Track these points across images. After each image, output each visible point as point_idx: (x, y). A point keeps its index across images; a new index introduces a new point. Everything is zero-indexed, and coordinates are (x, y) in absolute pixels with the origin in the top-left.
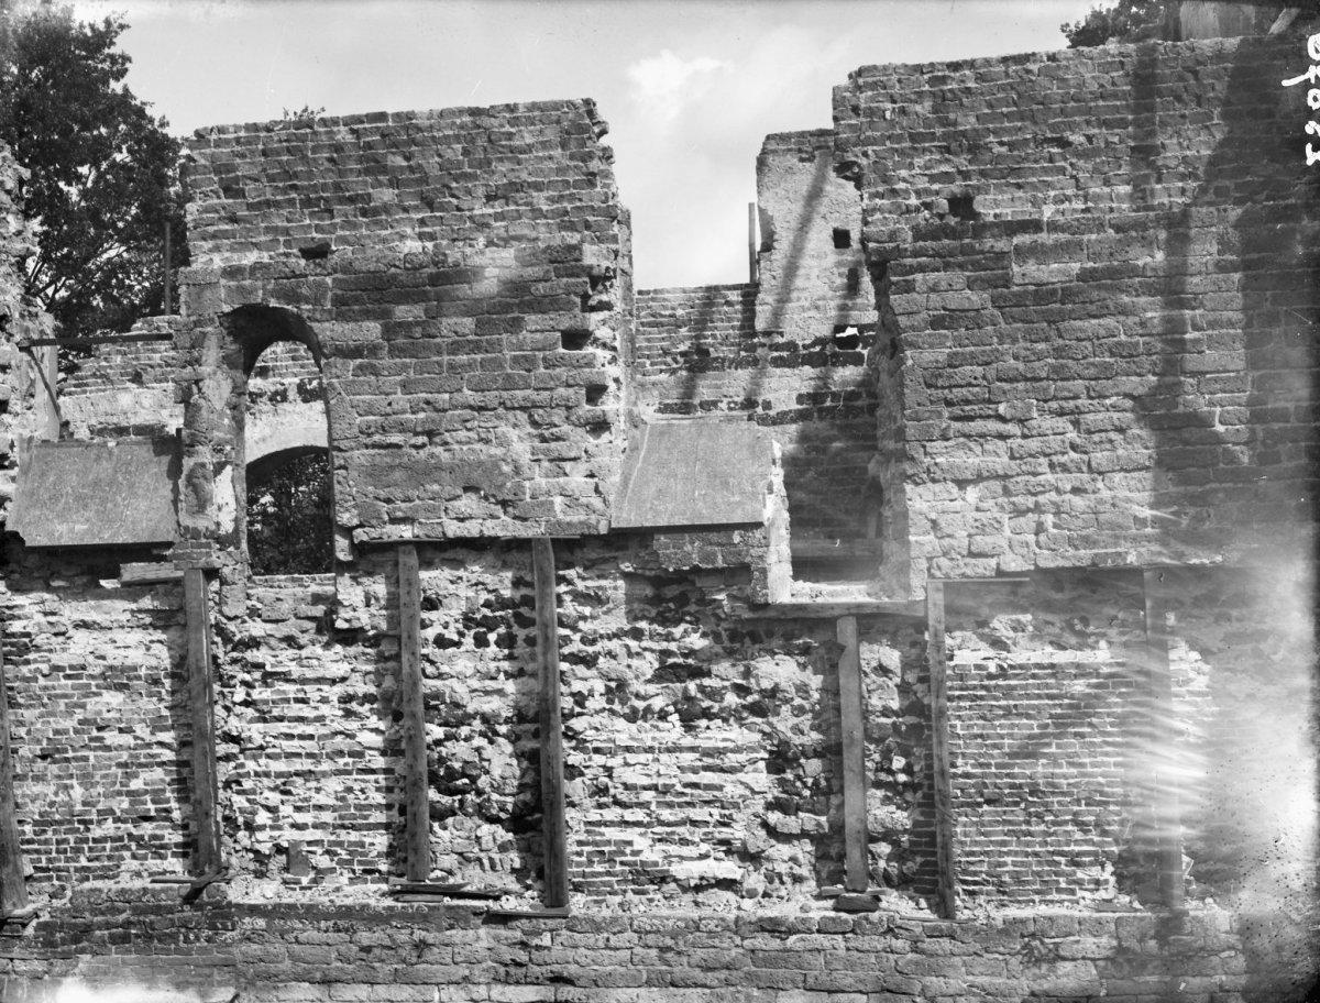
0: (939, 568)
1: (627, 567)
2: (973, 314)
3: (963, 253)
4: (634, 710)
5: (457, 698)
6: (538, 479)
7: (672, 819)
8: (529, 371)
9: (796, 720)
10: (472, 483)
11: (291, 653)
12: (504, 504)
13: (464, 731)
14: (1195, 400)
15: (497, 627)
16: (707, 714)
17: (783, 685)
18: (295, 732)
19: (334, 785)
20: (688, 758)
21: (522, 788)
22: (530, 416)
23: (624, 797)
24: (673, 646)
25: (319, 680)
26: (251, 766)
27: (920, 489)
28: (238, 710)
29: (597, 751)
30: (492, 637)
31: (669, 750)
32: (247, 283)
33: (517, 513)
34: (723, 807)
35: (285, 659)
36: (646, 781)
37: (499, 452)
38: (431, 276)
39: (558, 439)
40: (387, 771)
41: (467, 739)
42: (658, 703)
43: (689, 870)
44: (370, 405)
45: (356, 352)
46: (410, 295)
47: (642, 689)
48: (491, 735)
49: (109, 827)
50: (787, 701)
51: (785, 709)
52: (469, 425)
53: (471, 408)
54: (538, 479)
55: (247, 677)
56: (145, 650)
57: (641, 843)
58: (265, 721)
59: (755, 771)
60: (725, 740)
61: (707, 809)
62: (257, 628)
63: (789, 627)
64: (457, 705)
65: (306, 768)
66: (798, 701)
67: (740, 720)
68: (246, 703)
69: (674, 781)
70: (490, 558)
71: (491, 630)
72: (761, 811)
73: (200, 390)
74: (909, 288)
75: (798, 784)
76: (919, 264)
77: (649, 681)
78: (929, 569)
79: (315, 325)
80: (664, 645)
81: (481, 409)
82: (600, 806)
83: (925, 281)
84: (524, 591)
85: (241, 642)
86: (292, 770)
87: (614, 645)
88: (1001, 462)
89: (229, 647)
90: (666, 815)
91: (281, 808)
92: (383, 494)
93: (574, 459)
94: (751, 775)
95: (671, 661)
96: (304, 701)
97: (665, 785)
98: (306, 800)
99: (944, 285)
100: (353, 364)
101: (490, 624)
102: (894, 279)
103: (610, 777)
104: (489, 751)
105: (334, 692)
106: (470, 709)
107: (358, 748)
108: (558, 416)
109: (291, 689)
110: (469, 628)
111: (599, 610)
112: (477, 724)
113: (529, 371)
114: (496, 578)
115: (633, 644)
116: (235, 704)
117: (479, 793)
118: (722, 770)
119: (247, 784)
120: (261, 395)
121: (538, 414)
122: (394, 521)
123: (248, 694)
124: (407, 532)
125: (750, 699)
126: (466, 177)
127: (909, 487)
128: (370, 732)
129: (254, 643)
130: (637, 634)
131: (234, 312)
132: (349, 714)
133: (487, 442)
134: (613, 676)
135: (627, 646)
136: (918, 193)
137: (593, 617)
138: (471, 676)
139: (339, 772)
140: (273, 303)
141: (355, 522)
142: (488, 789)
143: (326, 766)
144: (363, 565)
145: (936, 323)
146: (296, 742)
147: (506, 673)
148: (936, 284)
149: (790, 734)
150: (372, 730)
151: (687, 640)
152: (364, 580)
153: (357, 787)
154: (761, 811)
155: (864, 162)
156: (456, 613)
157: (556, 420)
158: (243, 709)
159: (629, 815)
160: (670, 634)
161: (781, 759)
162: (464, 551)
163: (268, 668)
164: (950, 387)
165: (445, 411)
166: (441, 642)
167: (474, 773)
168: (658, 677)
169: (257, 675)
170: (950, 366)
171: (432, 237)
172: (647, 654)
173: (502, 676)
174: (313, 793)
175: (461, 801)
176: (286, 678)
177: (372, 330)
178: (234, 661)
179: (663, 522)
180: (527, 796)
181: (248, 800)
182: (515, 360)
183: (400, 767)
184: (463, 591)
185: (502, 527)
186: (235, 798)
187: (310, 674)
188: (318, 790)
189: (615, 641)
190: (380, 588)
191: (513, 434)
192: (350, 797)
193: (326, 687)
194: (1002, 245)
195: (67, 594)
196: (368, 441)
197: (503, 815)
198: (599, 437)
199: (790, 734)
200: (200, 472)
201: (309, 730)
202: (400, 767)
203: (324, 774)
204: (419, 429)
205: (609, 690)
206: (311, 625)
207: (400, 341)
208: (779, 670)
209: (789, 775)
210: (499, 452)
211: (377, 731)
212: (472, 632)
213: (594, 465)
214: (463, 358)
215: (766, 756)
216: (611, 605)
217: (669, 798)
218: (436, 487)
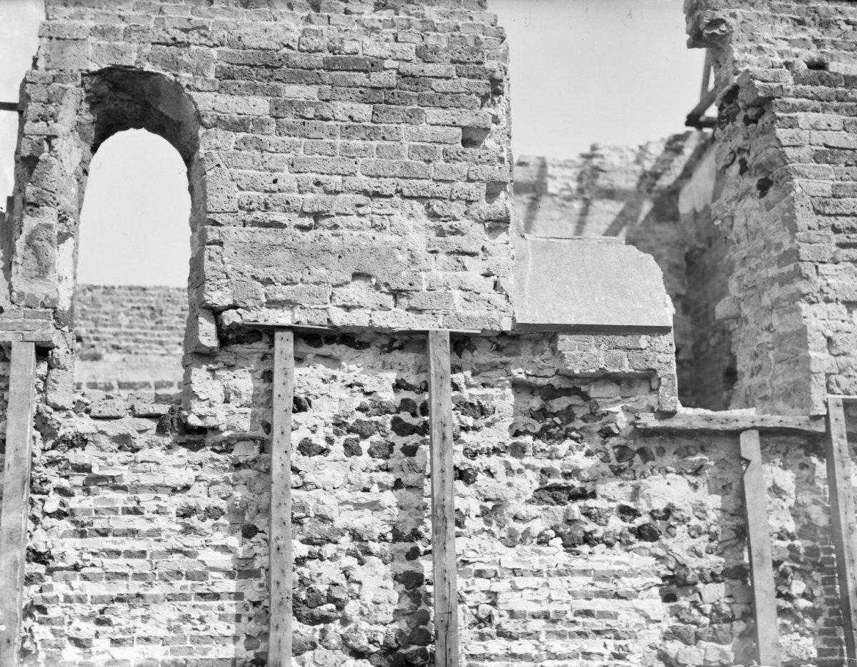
0: (838, 385)
1: (519, 373)
2: (849, 152)
3: (838, 99)
4: (512, 534)
5: (325, 511)
6: (434, 271)
7: (565, 651)
8: (429, 161)
9: (693, 542)
10: (363, 270)
11: (123, 456)
12: (397, 294)
13: (329, 549)
15: (372, 433)
16: (588, 539)
17: (677, 504)
18: (122, 548)
19: (167, 612)
20: (579, 582)
22: (429, 206)
23: (509, 626)
24: (556, 464)
25: (154, 488)
26: (60, 589)
27: (814, 307)
28: (47, 522)
29: (479, 574)
30: (365, 445)
31: (559, 574)
32: (120, 44)
33: (413, 304)
34: (618, 638)
35: (117, 464)
36: (536, 608)
37: (395, 240)
38: (326, 61)
39: (457, 232)
40: (238, 596)
41: (333, 558)
42: (537, 527)
44: (254, 180)
45: (239, 125)
46: (304, 75)
47: (523, 510)
50: (683, 521)
51: (681, 530)
52: (361, 210)
53: (365, 193)
54: (437, 271)
55: (65, 483)
58: (83, 534)
59: (650, 597)
60: (618, 563)
61: (600, 641)
62: (84, 425)
63: (684, 442)
64: (323, 519)
65: (133, 591)
66: (694, 522)
67: (627, 545)
68: (60, 515)
69: (566, 607)
70: (369, 355)
71: (364, 437)
72: (658, 642)
73: (51, 148)
74: (793, 124)
75: (695, 611)
76: (801, 104)
77: (530, 502)
78: (827, 386)
79: (195, 95)
80: (546, 463)
81: (376, 195)
82: (482, 637)
83: (807, 119)
84: (405, 394)
85: (64, 440)
86: (115, 594)
87: (494, 462)
89: (49, 444)
90: (557, 646)
91: (95, 641)
92: (262, 274)
93: (472, 254)
94: (647, 601)
95: (551, 481)
96: (136, 511)
97: (556, 612)
98: (129, 631)
99: (823, 125)
100: (236, 137)
102: (779, 114)
103: (494, 604)
105: (175, 503)
106: (339, 524)
107: (200, 568)
108: (457, 209)
109: (120, 499)
110: (337, 433)
111: (481, 422)
112: (346, 542)
113: (429, 161)
114: (375, 380)
115: (515, 463)
116: (46, 514)
117: (345, 621)
118: (617, 596)
119: (54, 612)
121: (437, 206)
122: (272, 304)
123: (62, 504)
124: (283, 317)
125: (638, 522)
127: (803, 305)
128: (217, 549)
129: (80, 441)
130: (518, 450)
131: (101, 73)
132: (188, 530)
133: (381, 228)
134: (491, 495)
135: (506, 463)
136: (781, 54)
137: (475, 429)
138: (339, 487)
139: (171, 598)
140: (148, 67)
141: (228, 301)
142: (356, 618)
143: (159, 589)
144: (224, 357)
145: (818, 157)
146: (122, 560)
147: (380, 484)
148: (816, 123)
149: (686, 557)
150: (216, 548)
151: (572, 457)
152: (223, 373)
153: (195, 614)
154: (658, 642)
155: (731, 21)
156: (328, 416)
157: (455, 212)
158: (54, 521)
159: (516, 647)
160: (553, 450)
161: (675, 585)
162: (343, 347)
163: (95, 471)
164: (835, 215)
165: (337, 193)
166: (306, 448)
167: (343, 596)
168: (537, 499)
169: (79, 479)
170: (834, 196)
172: (528, 472)
173: (375, 488)
174: (138, 623)
175: (323, 632)
176: (115, 485)
177: (259, 106)
178: (52, 462)
181: (54, 632)
182: (415, 150)
183: (252, 590)
184: (337, 390)
185: (398, 319)
186: (37, 628)
187: (146, 480)
188: (145, 619)
189: (494, 456)
190: (245, 382)
191: (410, 224)
192: (186, 628)
193: (164, 496)
196: (249, 218)
197: (373, 649)
198: (495, 237)
199: (686, 557)
200: (43, 234)
201: (138, 545)
202: (252, 590)
203: (156, 600)
204: (307, 209)
205: (485, 513)
206: (152, 425)
207: (289, 119)
208: (667, 488)
209: (684, 602)
210: (395, 240)
211: (225, 549)
212: (343, 439)
213: (490, 264)
214: (357, 143)
215: (660, 582)
216: (496, 416)
217: (559, 627)
218: (322, 271)
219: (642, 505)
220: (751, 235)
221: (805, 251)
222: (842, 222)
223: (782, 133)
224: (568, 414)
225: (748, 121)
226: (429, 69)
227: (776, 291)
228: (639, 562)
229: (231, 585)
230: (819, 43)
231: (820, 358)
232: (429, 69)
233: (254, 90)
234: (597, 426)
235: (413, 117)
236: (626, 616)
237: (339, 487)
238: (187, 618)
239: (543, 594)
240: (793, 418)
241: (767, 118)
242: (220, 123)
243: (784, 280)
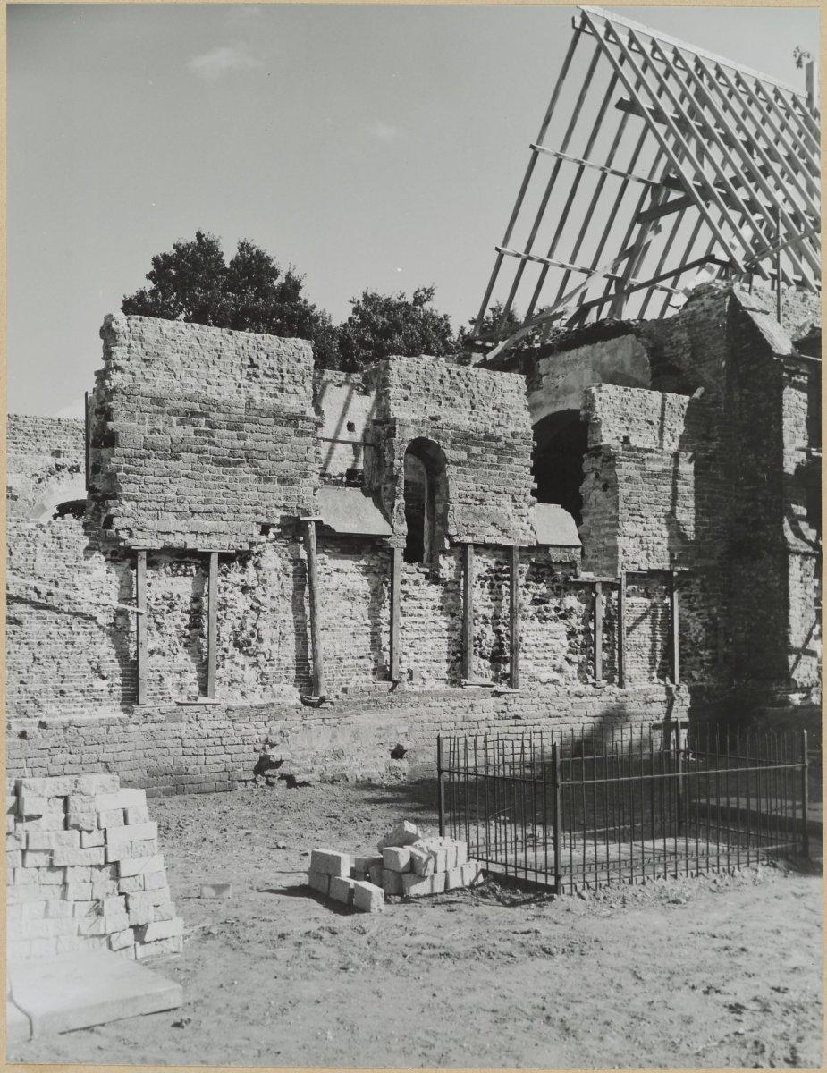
19: (431, 643)
42: (530, 613)
43: (544, 677)
45: (458, 464)
46: (476, 444)
51: (574, 616)
74: (620, 467)
88: (640, 532)
90: (539, 655)
101: (485, 579)
104: (486, 630)
106: (480, 612)
109: (416, 603)
112: (481, 619)
115: (526, 590)
120: (63, 467)
122: (468, 534)
140: (430, 438)
145: (627, 480)
161: (571, 634)
168: (532, 604)
176: (414, 598)
177: (463, 455)
179: (554, 543)
180: (497, 648)
187: (424, 596)
195: (332, 556)
208: (571, 601)
214: (493, 472)
219: (563, 607)
223: (617, 470)
225: (603, 461)
226: (515, 441)
227: (607, 530)
228: (560, 628)
229: (446, 634)
230: (627, 429)
232: (515, 441)
236: (557, 646)
237: (479, 598)
242: (452, 462)
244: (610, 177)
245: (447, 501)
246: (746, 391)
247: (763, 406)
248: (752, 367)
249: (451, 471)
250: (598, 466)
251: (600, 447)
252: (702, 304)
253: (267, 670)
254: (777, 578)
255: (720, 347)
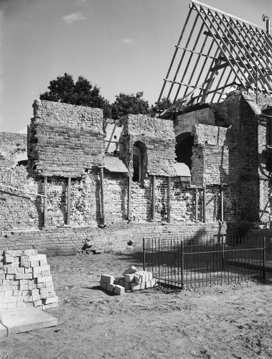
14: (224, 167)
16: (179, 200)
19: (141, 208)
21: (163, 208)
25: (139, 193)
36: (175, 208)
42: (174, 198)
43: (179, 219)
45: (151, 149)
48: (159, 201)
49: (114, 213)
51: (189, 199)
54: (169, 169)
56: (118, 189)
57: (174, 216)
64: (156, 197)
70: (161, 178)
88: (211, 172)
90: (177, 212)
101: (159, 187)
104: (159, 204)
109: (136, 195)
112: (158, 200)
115: (173, 191)
120: (20, 149)
122: (154, 172)
125: (184, 198)
126: (160, 128)
133: (164, 163)
138: (157, 193)
143: (140, 205)
145: (206, 155)
168: (175, 195)
171: (156, 135)
176: (136, 193)
177: (152, 147)
179: (182, 175)
180: (163, 210)
185: (166, 175)
187: (139, 192)
194: (212, 147)
195: (109, 179)
208: (188, 194)
214: (162, 152)
219: (185, 196)
220: (197, 163)
221: (204, 167)
222: (208, 164)
224: (179, 185)
225: (199, 149)
227: (200, 171)
228: (184, 203)
229: (146, 205)
230: (207, 138)
231: (204, 181)
233: (152, 144)
234: (181, 187)
235: (168, 149)
238: (143, 209)
239: (176, 206)
240: (201, 187)
241: (201, 149)
243: (201, 170)
244: (201, 56)
245: (147, 162)
246: (246, 126)
247: (252, 131)
248: (248, 119)
249: (148, 152)
250: (197, 151)
251: (198, 144)
252: (232, 98)
253: (87, 216)
254: (256, 187)
255: (238, 112)
